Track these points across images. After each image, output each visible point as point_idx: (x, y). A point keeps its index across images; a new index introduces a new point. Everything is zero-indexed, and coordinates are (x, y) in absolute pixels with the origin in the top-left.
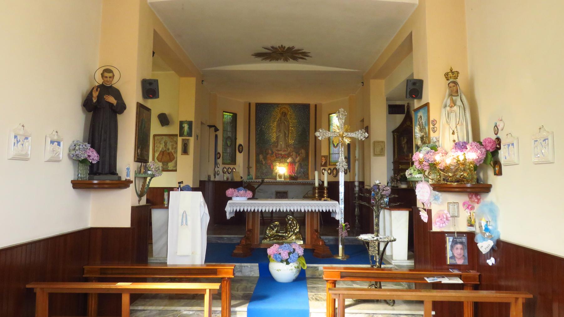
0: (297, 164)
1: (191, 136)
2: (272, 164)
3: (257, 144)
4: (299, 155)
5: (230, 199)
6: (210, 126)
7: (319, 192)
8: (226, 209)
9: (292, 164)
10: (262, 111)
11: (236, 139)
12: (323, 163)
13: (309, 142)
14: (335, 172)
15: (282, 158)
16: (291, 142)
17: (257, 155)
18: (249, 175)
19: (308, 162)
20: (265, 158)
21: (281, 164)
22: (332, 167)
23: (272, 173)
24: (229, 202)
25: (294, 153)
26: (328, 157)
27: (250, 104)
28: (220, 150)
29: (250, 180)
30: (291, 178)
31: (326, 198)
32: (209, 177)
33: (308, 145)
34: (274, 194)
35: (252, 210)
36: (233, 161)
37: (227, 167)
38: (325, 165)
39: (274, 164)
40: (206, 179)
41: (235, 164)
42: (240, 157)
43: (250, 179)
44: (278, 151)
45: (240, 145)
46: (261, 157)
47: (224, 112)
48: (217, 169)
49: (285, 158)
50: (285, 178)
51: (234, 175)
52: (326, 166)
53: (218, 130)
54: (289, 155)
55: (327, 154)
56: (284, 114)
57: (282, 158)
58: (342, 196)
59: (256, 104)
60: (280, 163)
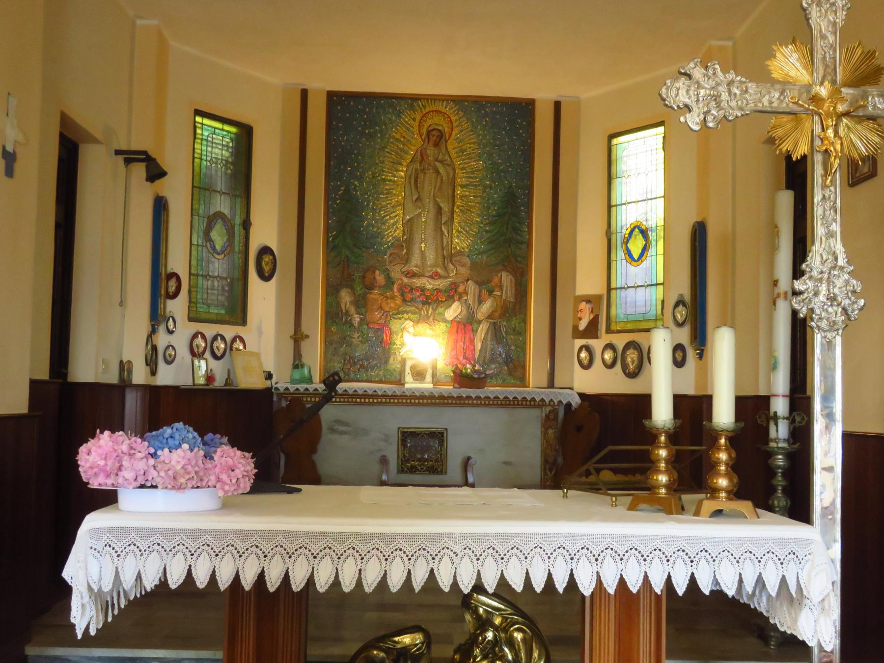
0: (482, 330)
1: (439, 436)
2: (386, 325)
3: (331, 247)
4: (491, 292)
5: (107, 499)
6: (130, 157)
7: (675, 461)
8: (67, 573)
9: (464, 326)
10: (353, 122)
11: (246, 224)
12: (583, 325)
13: (529, 244)
14: (632, 356)
15: (428, 302)
16: (460, 243)
17: (332, 290)
18: (296, 367)
19: (525, 321)
20: (361, 303)
21: (423, 328)
22: (620, 341)
23: (386, 362)
24: (93, 521)
25: (471, 286)
26: (600, 303)
27: (304, 93)
28: (178, 260)
29: (302, 387)
30: (461, 378)
31: (722, 501)
32: (125, 367)
33: (527, 258)
34: (395, 439)
35: (248, 582)
36: (237, 311)
37: (209, 335)
38: (592, 331)
39: (395, 325)
40: (112, 378)
41: (243, 322)
42: (264, 298)
43: (301, 381)
44: (412, 275)
45: (265, 250)
46: (346, 297)
47: (198, 113)
48: (162, 340)
49: (438, 302)
50: (436, 381)
51: (240, 362)
52: (595, 336)
53: (162, 174)
54: (452, 294)
55: (600, 290)
56: (437, 138)
57: (426, 303)
58: (827, 487)
59: (331, 95)
60: (417, 322)
